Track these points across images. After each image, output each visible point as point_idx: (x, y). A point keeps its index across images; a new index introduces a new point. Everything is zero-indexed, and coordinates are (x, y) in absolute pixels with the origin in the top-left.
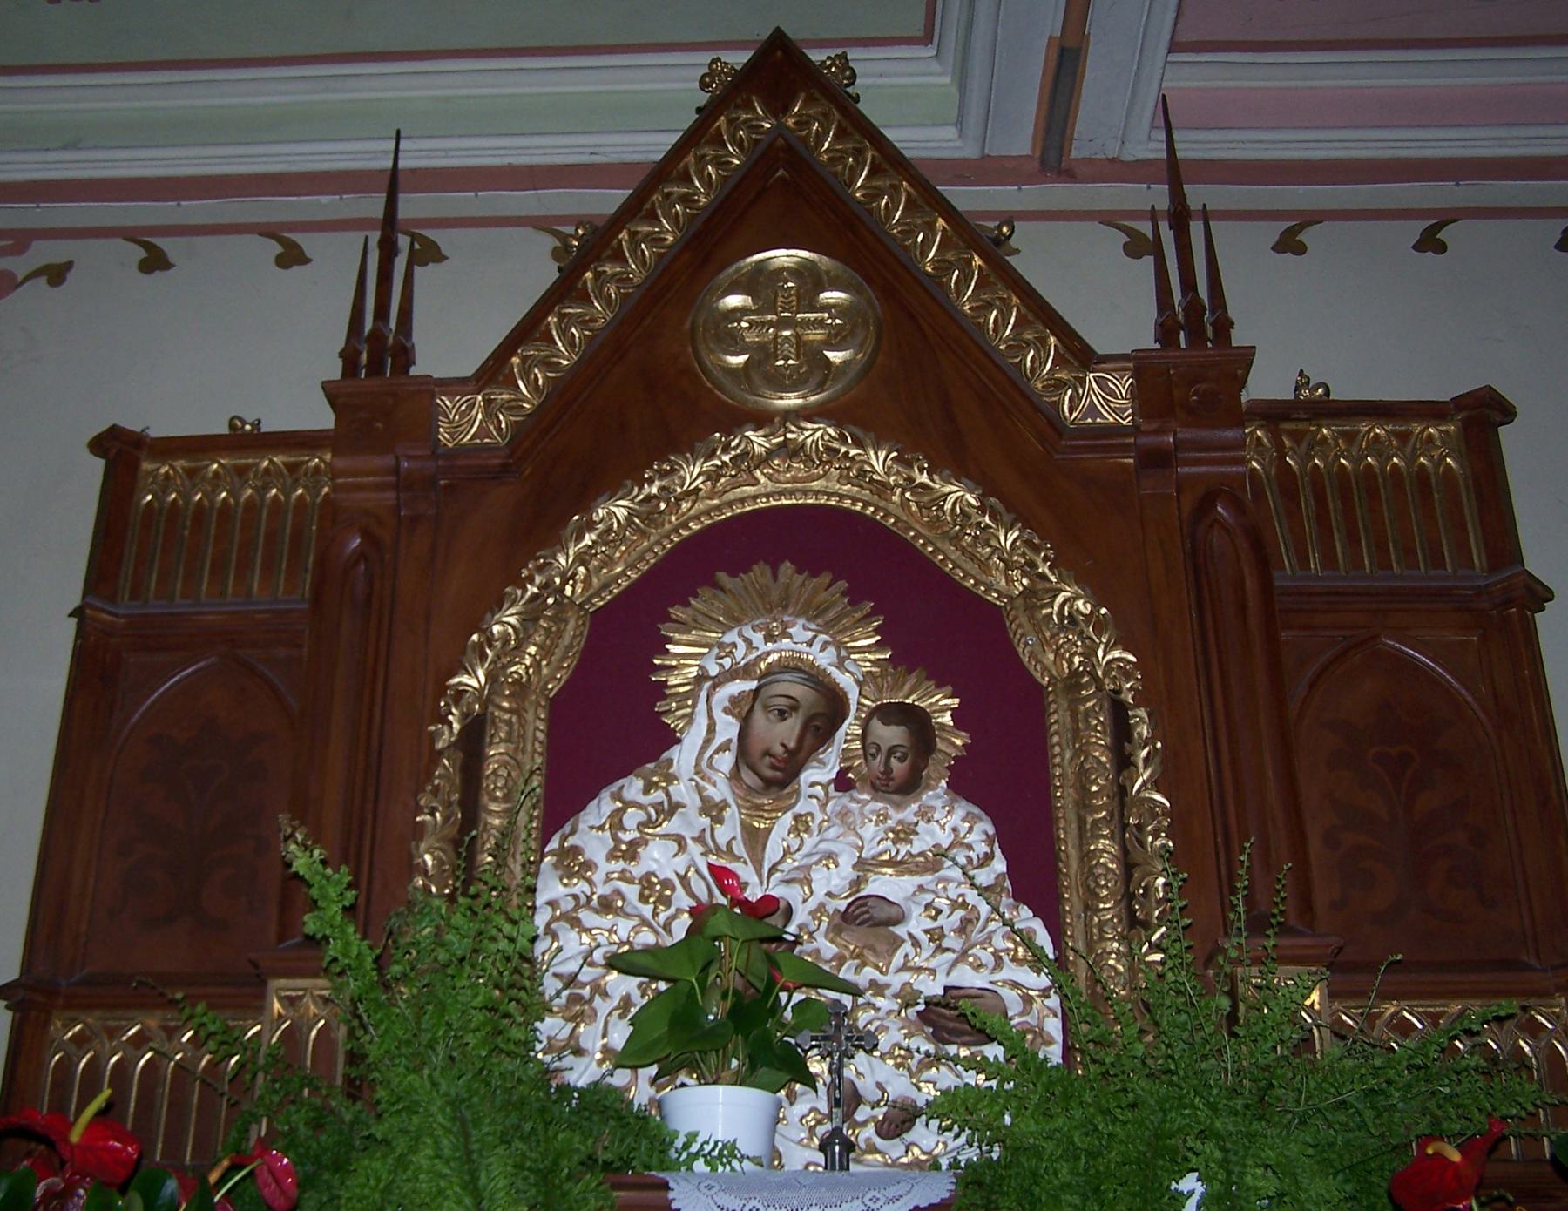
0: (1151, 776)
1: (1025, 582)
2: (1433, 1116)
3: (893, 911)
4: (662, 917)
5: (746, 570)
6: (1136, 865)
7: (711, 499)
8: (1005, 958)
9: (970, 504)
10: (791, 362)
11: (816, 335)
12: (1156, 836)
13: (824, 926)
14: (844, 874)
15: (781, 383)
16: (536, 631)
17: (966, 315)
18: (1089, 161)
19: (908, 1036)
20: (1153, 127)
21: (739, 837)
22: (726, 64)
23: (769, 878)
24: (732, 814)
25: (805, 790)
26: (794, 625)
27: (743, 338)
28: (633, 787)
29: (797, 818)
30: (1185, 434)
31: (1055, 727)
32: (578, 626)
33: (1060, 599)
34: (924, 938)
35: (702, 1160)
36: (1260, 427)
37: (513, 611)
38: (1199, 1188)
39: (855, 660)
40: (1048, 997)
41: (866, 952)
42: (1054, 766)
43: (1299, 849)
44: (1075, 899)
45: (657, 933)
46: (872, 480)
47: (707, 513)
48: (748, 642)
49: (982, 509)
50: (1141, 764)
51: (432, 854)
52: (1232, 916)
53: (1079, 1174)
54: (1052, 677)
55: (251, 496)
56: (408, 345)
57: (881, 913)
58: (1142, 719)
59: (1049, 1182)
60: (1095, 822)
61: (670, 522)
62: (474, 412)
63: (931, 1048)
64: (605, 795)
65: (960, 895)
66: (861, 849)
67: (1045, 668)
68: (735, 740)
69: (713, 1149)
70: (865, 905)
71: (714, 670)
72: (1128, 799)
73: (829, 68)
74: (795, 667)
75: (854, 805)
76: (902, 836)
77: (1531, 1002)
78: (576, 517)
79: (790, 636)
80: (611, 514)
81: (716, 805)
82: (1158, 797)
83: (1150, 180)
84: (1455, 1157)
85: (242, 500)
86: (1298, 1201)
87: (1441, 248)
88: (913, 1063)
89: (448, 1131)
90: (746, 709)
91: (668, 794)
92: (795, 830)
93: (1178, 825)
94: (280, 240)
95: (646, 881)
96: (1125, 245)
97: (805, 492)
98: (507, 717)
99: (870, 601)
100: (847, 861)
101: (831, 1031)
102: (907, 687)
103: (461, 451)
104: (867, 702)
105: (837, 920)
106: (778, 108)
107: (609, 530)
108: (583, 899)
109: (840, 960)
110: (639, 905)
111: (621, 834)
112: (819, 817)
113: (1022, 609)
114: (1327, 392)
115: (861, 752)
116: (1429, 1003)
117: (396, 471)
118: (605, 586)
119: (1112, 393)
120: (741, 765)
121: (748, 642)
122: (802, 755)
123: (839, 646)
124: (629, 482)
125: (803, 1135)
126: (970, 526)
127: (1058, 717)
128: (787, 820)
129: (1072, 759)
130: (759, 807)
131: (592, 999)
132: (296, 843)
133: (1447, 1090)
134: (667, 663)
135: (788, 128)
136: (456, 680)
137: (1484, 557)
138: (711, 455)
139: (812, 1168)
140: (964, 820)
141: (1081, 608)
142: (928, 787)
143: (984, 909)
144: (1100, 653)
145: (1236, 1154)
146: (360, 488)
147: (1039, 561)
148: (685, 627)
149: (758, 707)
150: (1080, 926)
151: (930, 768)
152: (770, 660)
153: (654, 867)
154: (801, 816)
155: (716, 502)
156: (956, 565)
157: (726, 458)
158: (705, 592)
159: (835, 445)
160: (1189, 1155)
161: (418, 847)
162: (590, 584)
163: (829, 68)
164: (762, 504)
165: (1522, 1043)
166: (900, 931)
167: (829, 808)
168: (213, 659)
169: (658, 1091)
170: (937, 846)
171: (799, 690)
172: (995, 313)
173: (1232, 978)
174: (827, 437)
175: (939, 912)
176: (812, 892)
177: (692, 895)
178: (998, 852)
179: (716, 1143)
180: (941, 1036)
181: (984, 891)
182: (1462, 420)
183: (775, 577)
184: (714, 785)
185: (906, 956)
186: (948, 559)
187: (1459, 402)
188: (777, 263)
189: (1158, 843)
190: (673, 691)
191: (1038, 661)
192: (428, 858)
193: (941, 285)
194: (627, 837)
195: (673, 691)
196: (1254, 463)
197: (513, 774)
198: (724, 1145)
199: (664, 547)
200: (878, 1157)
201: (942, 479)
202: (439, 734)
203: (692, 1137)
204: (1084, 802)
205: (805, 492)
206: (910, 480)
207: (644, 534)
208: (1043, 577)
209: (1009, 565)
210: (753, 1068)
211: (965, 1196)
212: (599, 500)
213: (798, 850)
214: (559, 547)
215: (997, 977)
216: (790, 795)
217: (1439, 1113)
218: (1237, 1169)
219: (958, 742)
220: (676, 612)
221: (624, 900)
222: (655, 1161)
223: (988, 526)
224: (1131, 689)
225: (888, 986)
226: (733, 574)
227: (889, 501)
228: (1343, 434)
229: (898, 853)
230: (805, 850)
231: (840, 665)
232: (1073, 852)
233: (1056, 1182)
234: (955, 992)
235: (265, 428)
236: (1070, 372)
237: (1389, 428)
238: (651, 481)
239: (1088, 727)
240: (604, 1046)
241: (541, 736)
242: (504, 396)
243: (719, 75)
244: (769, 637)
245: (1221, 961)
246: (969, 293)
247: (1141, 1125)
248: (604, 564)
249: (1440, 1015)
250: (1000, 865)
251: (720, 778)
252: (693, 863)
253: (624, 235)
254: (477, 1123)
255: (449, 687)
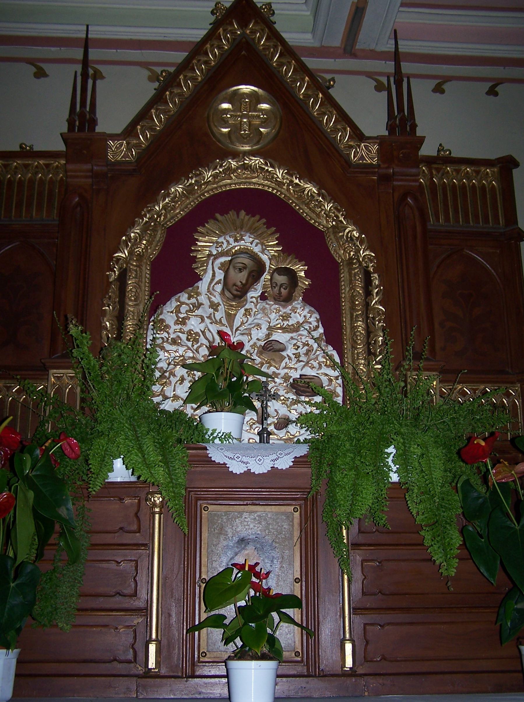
0: (378, 299)
1: (334, 223)
2: (473, 426)
3: (281, 346)
4: (195, 346)
5: (227, 213)
6: (371, 332)
7: (214, 184)
8: (323, 365)
9: (314, 192)
10: (247, 132)
11: (257, 122)
12: (379, 322)
13: (256, 351)
14: (263, 332)
15: (244, 140)
16: (146, 235)
17: (315, 117)
18: (363, 50)
19: (287, 393)
20: (389, 38)
21: (224, 317)
22: (223, 5)
23: (235, 333)
24: (221, 308)
25: (249, 300)
26: (245, 236)
27: (228, 121)
28: (184, 297)
29: (246, 310)
30: (397, 169)
31: (343, 279)
32: (162, 233)
33: (347, 231)
34: (293, 357)
35: (218, 439)
36: (424, 166)
37: (138, 228)
38: (394, 451)
39: (268, 250)
40: (338, 379)
41: (307, 385)
42: (342, 293)
43: (432, 331)
44: (348, 343)
45: (193, 352)
46: (277, 181)
47: (212, 190)
48: (228, 242)
49: (319, 195)
50: (375, 295)
51: (109, 322)
52: (407, 353)
53: (352, 446)
54: (342, 259)
55: (31, 177)
56: (95, 119)
57: (277, 346)
58: (376, 278)
59: (343, 449)
60: (357, 315)
61: (198, 193)
62: (123, 148)
63: (295, 397)
64: (173, 299)
65: (306, 341)
66: (270, 323)
67: (340, 256)
68: (223, 280)
69: (222, 435)
70: (271, 344)
71: (215, 252)
72: (369, 308)
73: (264, 9)
74: (245, 252)
75: (267, 306)
76: (285, 318)
77: (508, 385)
78: (163, 191)
79: (244, 240)
80: (176, 190)
81: (215, 304)
82: (381, 307)
83: (386, 60)
84: (483, 443)
85: (27, 178)
86: (428, 456)
87: (496, 94)
88: (288, 403)
89: (129, 429)
90: (227, 267)
91: (197, 300)
92: (245, 315)
93: (388, 318)
94: (35, 66)
95: (189, 333)
96: (375, 87)
97: (250, 183)
98: (135, 268)
99: (274, 227)
100: (264, 327)
101: (263, 393)
102: (288, 261)
103: (117, 163)
104: (273, 267)
105: (261, 349)
106: (243, 25)
107: (175, 196)
108: (165, 339)
109: (262, 364)
110: (187, 342)
111: (179, 315)
112: (254, 310)
113: (332, 232)
114: (450, 153)
115: (270, 286)
116: (472, 385)
117: (92, 171)
118: (172, 218)
119: (370, 152)
120: (224, 289)
121: (228, 242)
122: (248, 286)
123: (262, 244)
124: (183, 178)
125: (248, 428)
126: (314, 201)
127: (344, 275)
128: (242, 311)
129: (349, 291)
130: (232, 306)
131: (169, 377)
132: (73, 324)
133: (478, 417)
134: (197, 249)
135: (247, 34)
136: (117, 255)
137: (504, 221)
138: (215, 169)
139: (251, 441)
140: (308, 313)
141: (355, 234)
142: (295, 300)
143: (315, 346)
144: (361, 252)
145: (408, 440)
146: (77, 177)
147: (340, 216)
148: (203, 235)
149: (231, 267)
150: (350, 354)
151: (296, 292)
152: (236, 249)
153: (192, 328)
154: (247, 309)
155: (215, 186)
156: (307, 215)
157: (221, 170)
158: (211, 221)
159: (263, 166)
160: (392, 440)
161: (103, 320)
162: (167, 217)
163: (264, 9)
164: (233, 187)
165: (504, 400)
166: (284, 354)
167: (258, 307)
168: (17, 243)
169: (194, 412)
170: (298, 322)
171: (247, 261)
172: (326, 117)
173: (406, 375)
174: (260, 163)
175: (299, 347)
176: (251, 338)
177: (207, 339)
178: (320, 325)
179: (223, 433)
180: (298, 393)
181: (316, 340)
182: (500, 167)
183: (238, 217)
184: (215, 297)
185: (286, 363)
186: (304, 211)
187: (499, 160)
188: (242, 91)
189: (380, 324)
190: (199, 260)
191: (337, 253)
192: (108, 323)
193: (306, 103)
194: (182, 316)
195: (199, 260)
196: (421, 180)
197: (138, 291)
198: (226, 434)
199: (195, 203)
200: (275, 436)
201: (304, 181)
202: (110, 276)
203: (214, 431)
204: (353, 308)
205: (250, 183)
206: (292, 181)
207: (188, 198)
208: (341, 221)
209: (327, 216)
210: (235, 405)
211: (313, 453)
212: (172, 185)
213: (246, 322)
214: (156, 203)
215: (320, 372)
216: (243, 302)
217: (476, 425)
218: (408, 445)
219: (307, 283)
220: (200, 229)
221: (181, 340)
222: (200, 439)
223: (321, 201)
224: (372, 266)
225: (279, 374)
226: (222, 215)
227: (282, 188)
228: (455, 170)
229: (284, 324)
230: (249, 322)
231: (263, 252)
232: (348, 326)
233: (345, 449)
234: (304, 377)
235: (36, 149)
236: (354, 142)
237: (473, 169)
238: (192, 178)
239: (356, 280)
240: (174, 394)
241: (148, 276)
242: (135, 142)
243: (220, 10)
244: (236, 240)
245: (402, 369)
246: (317, 108)
247: (375, 429)
248: (172, 209)
249: (477, 389)
250: (321, 330)
251: (216, 294)
252: (207, 327)
253: (181, 77)
254: (139, 427)
255: (114, 257)
